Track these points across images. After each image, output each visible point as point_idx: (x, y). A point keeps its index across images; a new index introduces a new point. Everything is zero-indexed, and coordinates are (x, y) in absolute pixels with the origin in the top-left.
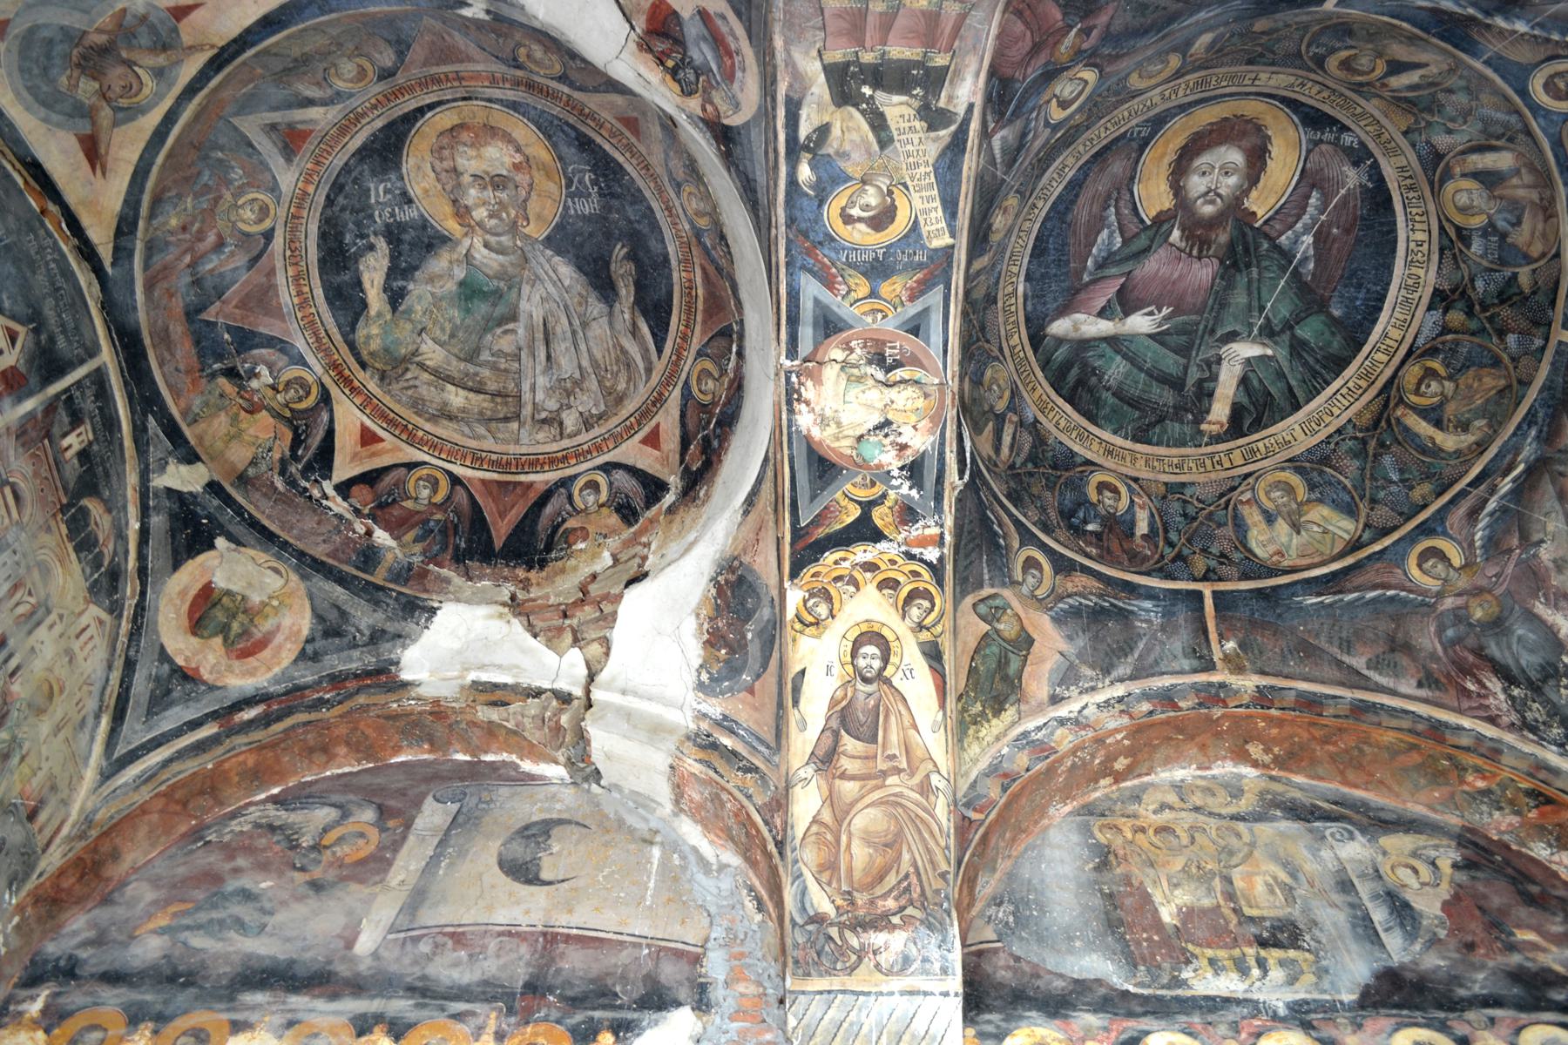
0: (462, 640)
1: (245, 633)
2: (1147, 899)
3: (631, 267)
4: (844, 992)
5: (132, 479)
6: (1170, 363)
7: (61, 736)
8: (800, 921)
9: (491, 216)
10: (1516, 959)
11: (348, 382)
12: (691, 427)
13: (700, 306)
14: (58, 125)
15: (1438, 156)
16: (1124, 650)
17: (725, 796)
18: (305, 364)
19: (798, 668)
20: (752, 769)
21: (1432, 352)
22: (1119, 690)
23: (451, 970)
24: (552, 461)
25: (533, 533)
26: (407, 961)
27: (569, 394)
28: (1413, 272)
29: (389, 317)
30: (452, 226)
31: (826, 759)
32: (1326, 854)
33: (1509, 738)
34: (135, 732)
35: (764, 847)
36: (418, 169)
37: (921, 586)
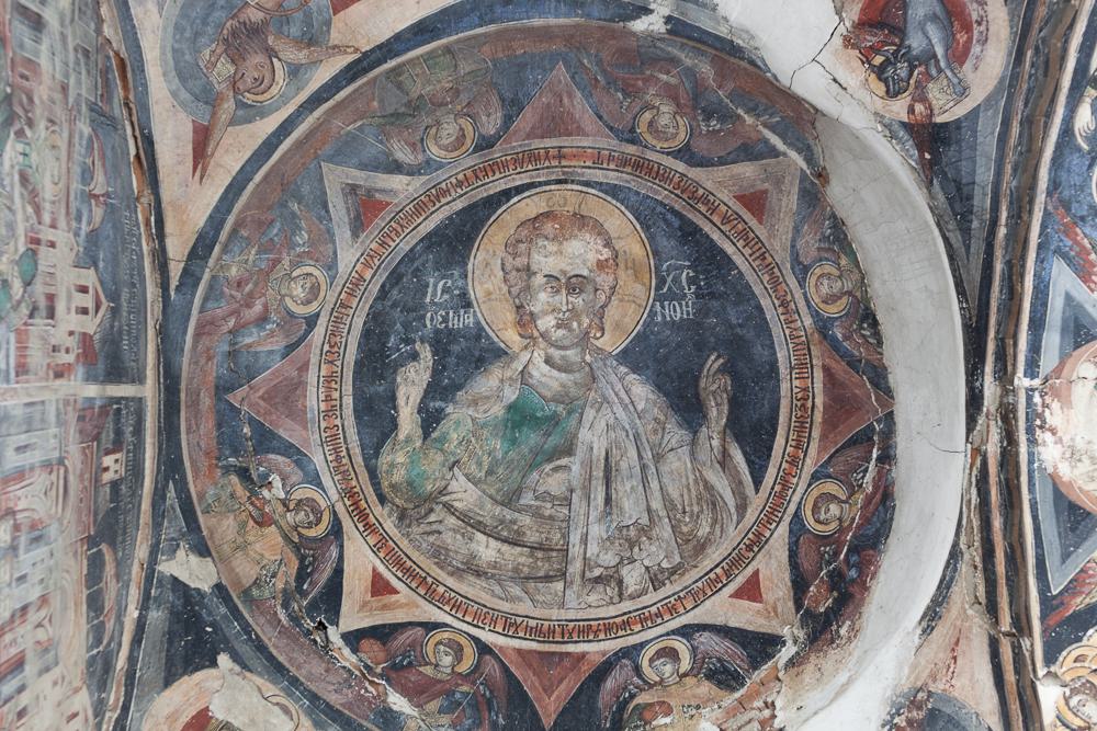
3: (726, 381)
5: (142, 552)
9: (558, 326)
11: (363, 516)
12: (806, 564)
13: (818, 417)
14: (183, 104)
18: (320, 485)
24: (608, 629)
25: (593, 709)
29: (418, 444)
30: (511, 337)
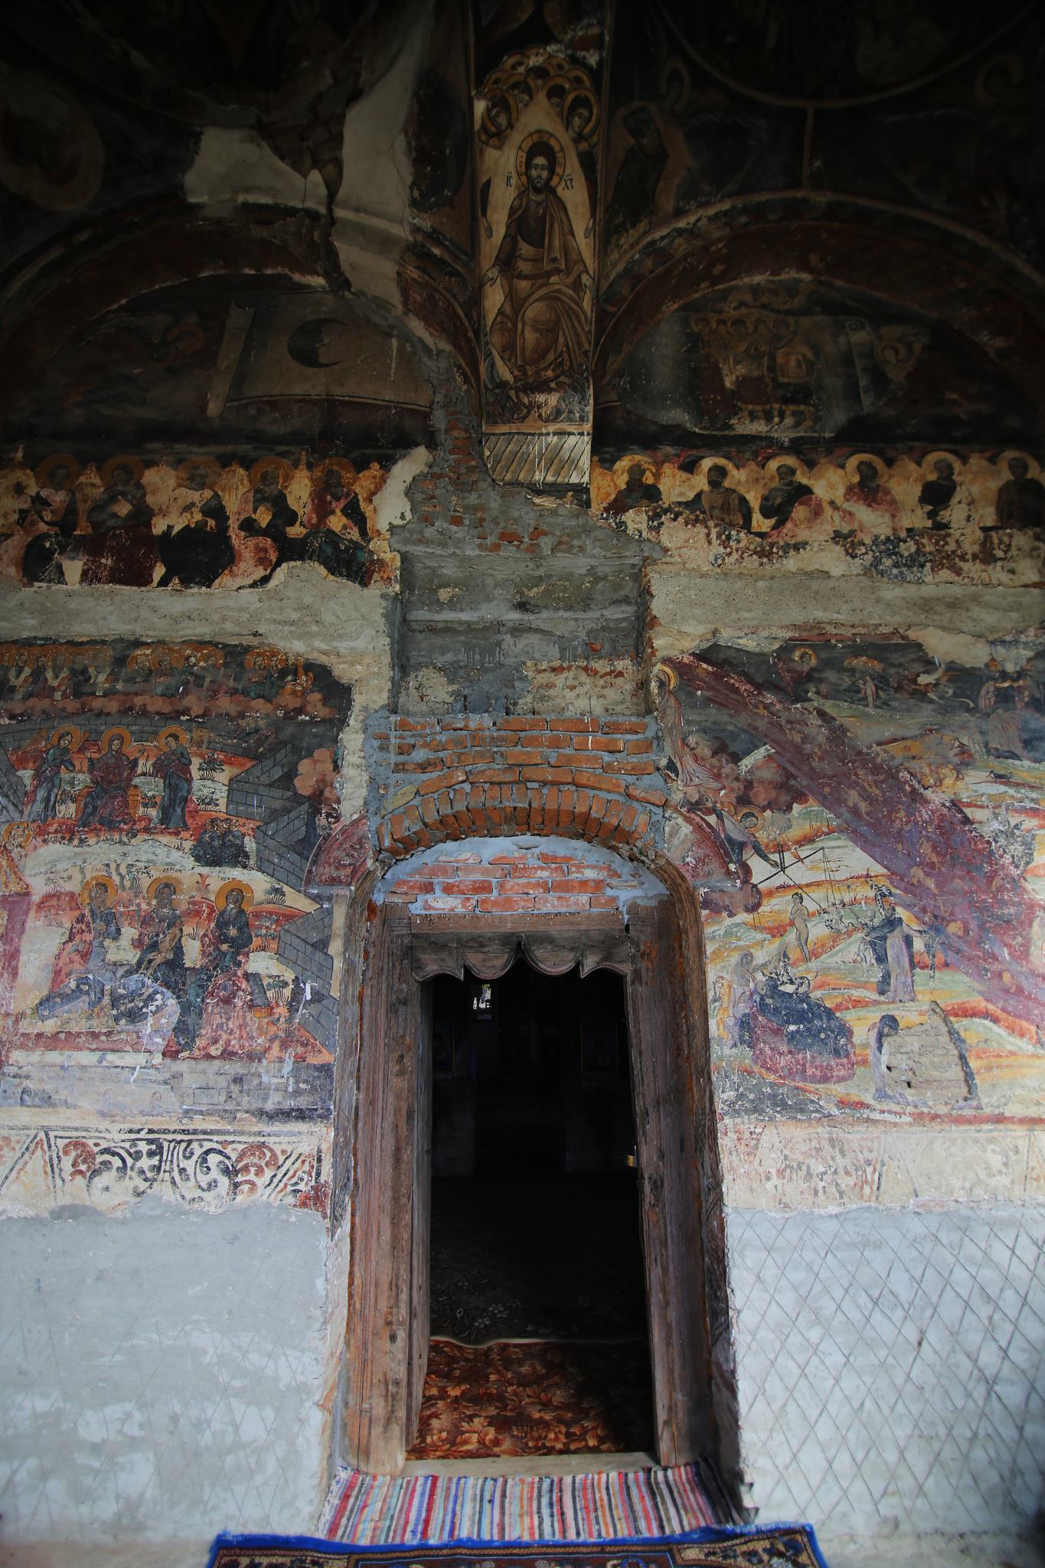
2: (718, 371)
8: (490, 386)
17: (437, 296)
19: (484, 179)
20: (455, 274)
22: (726, 206)
23: (271, 424)
31: (506, 261)
32: (842, 340)
35: (464, 332)
37: (583, 93)
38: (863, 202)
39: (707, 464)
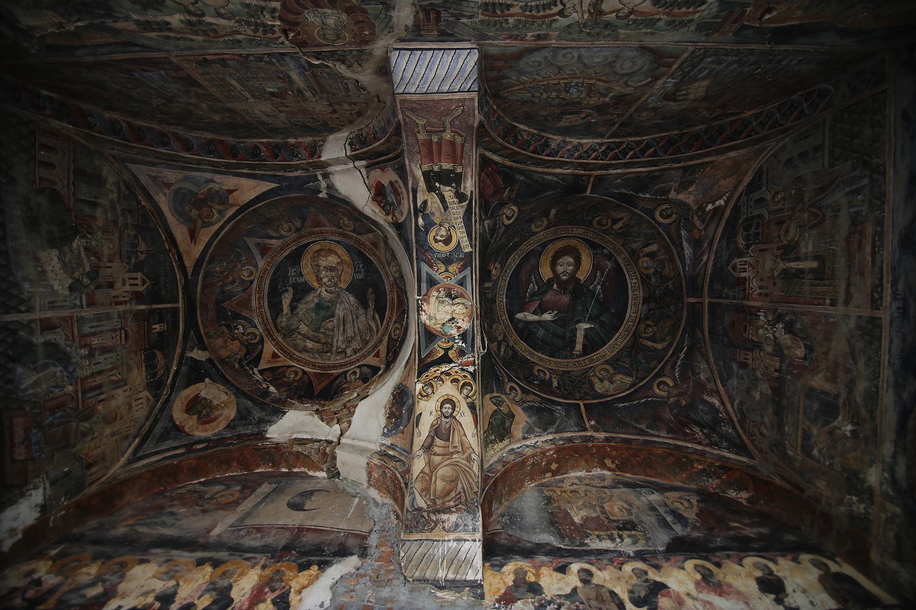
0: (295, 424)
1: (208, 415)
3: (373, 296)
4: (427, 540)
5: (178, 351)
6: (559, 330)
7: (114, 438)
10: (732, 533)
11: (271, 336)
15: (634, 251)
16: (552, 423)
21: (647, 318)
22: (551, 437)
26: (233, 537)
27: (350, 342)
28: (635, 294)
30: (316, 284)
31: (428, 447)
32: (643, 498)
33: (707, 449)
34: (149, 447)
36: (306, 266)
38: (623, 436)
39: (575, 567)
